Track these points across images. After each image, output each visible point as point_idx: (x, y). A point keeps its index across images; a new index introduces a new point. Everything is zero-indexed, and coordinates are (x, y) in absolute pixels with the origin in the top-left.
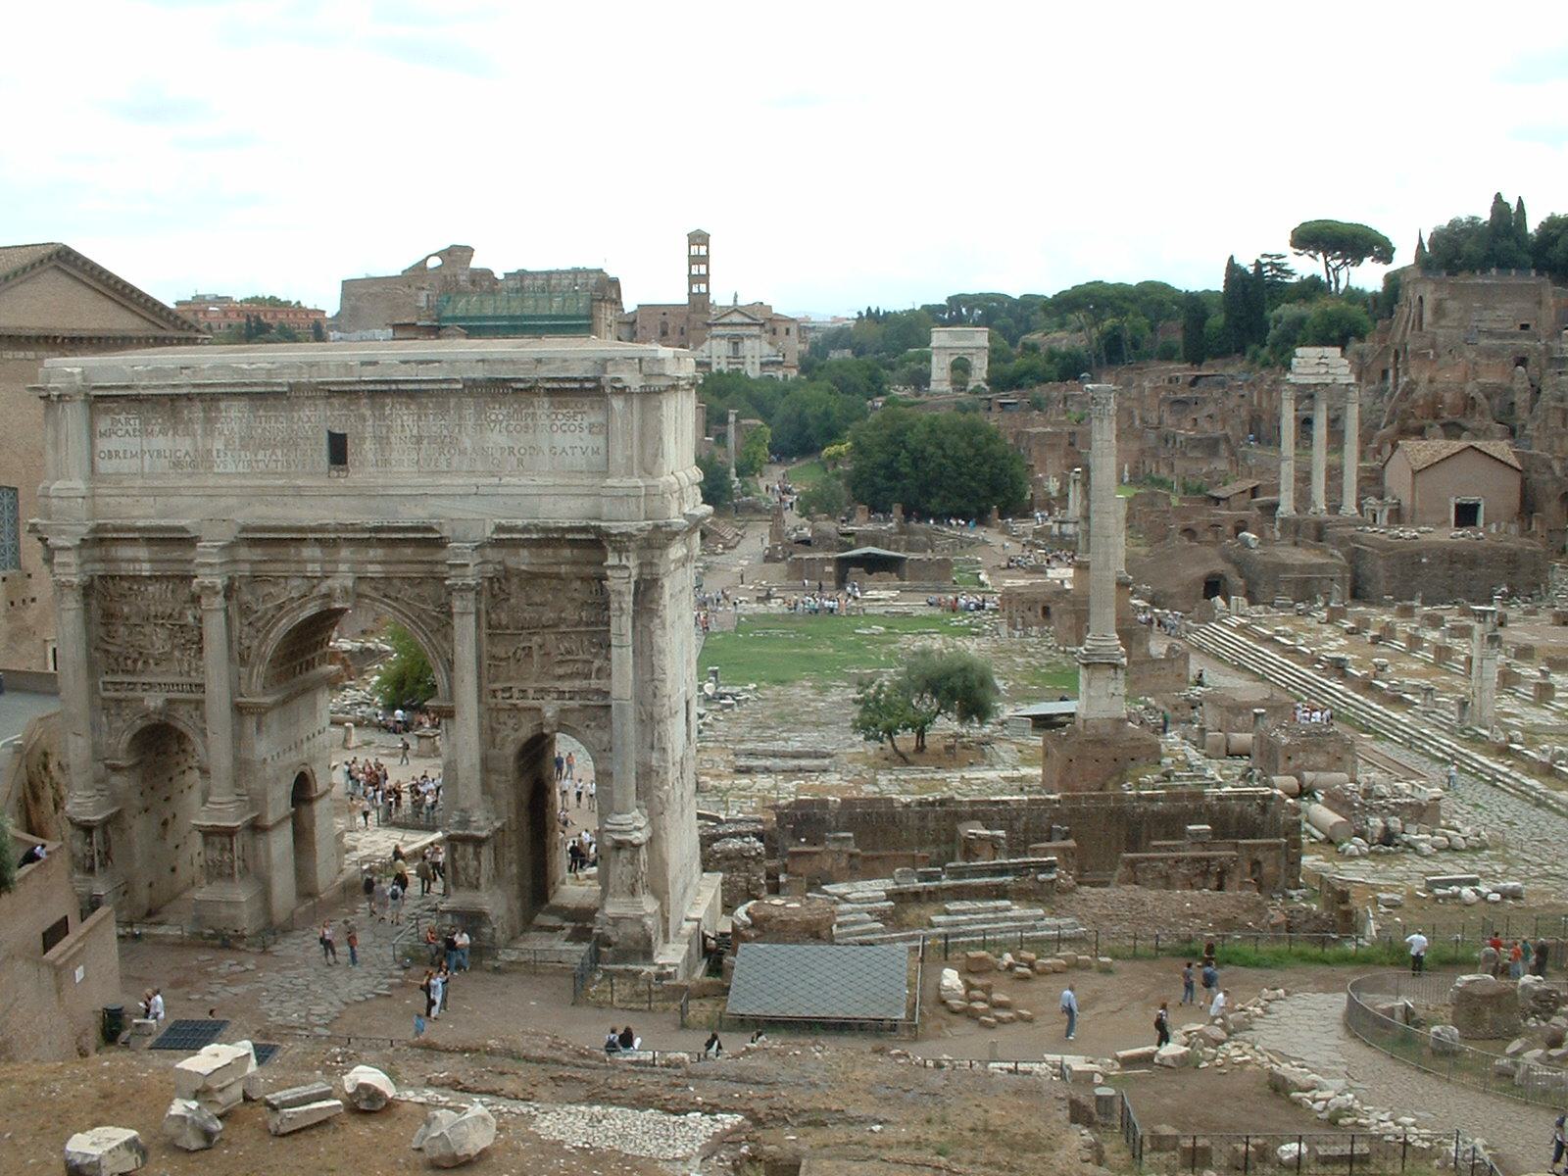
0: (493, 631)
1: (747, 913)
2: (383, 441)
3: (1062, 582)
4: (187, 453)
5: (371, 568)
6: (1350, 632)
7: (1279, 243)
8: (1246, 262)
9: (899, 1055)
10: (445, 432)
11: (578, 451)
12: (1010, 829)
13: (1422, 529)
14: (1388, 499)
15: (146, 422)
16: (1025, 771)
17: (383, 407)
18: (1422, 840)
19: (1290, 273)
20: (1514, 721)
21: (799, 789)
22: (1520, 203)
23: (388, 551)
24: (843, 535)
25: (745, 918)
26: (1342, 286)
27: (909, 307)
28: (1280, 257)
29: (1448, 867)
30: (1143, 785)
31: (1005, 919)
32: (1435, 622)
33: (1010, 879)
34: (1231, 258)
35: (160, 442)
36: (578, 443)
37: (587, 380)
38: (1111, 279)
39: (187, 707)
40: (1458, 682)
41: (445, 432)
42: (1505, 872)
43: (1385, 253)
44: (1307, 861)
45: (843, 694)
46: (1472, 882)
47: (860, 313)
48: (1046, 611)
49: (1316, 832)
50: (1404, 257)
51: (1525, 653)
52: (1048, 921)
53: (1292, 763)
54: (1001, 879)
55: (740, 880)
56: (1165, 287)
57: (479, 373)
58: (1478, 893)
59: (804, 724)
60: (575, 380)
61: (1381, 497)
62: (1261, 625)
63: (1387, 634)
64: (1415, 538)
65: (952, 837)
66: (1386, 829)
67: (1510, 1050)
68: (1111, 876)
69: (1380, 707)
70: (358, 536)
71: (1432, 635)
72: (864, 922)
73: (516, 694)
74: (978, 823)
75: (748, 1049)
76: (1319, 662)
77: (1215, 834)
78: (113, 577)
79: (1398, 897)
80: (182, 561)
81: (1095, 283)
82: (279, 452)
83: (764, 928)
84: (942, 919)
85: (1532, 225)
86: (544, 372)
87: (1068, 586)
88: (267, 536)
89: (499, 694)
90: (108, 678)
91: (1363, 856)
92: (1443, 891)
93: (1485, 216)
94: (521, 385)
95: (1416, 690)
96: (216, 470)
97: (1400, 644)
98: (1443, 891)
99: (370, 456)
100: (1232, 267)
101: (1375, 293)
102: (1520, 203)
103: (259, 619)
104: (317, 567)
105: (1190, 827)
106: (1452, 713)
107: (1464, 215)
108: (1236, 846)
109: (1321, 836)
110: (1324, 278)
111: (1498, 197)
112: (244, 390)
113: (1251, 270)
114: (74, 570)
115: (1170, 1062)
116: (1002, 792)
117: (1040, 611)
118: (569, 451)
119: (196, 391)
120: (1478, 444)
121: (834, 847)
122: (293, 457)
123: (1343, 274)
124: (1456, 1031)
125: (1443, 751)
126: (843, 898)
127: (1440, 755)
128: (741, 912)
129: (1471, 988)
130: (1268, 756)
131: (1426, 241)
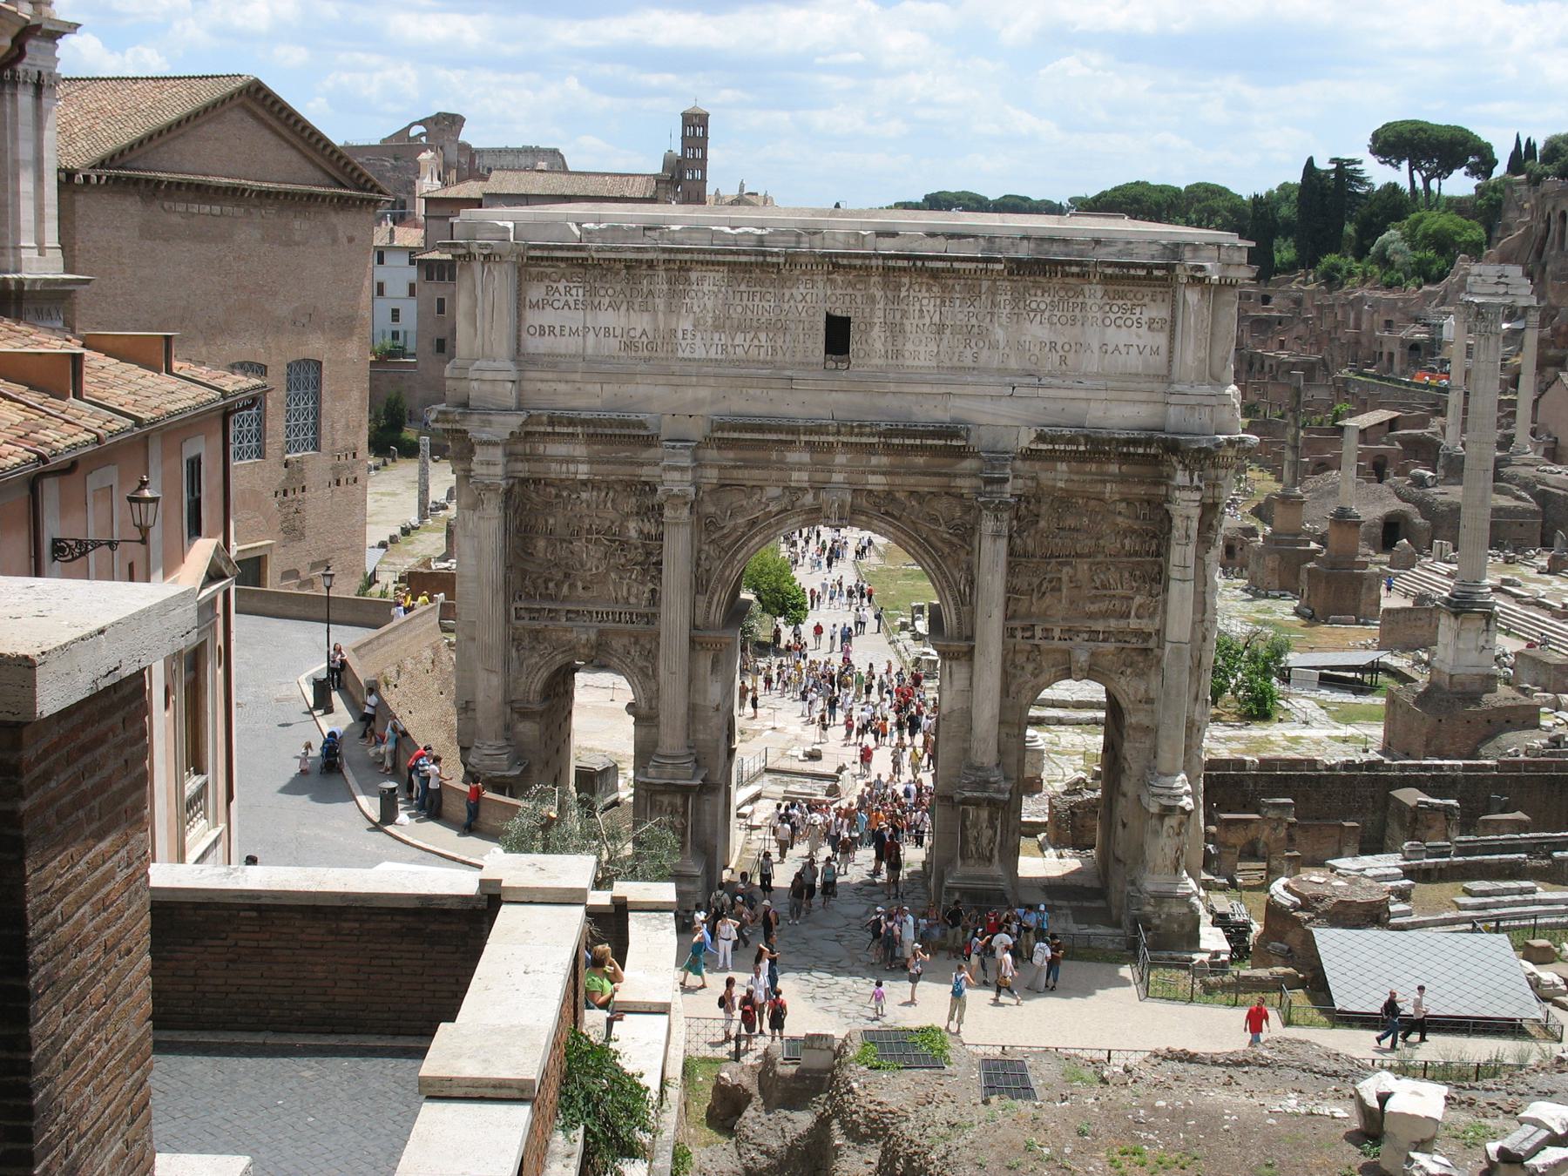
0: (1015, 559)
2: (895, 330)
4: (644, 332)
5: (872, 479)
7: (1358, 150)
10: (974, 321)
11: (1134, 350)
15: (593, 292)
17: (898, 287)
23: (896, 460)
31: (1534, 902)
35: (607, 318)
36: (1135, 341)
37: (1158, 267)
39: (625, 641)
41: (974, 321)
57: (1024, 252)
60: (1143, 266)
70: (864, 440)
73: (1038, 633)
78: (537, 482)
80: (632, 463)
82: (763, 336)
86: (1102, 254)
88: (748, 436)
89: (1019, 634)
90: (520, 605)
94: (1075, 269)
96: (680, 354)
99: (878, 345)
103: (724, 537)
104: (805, 476)
112: (858, 262)
114: (499, 470)
118: (1124, 350)
119: (666, 256)
122: (780, 342)
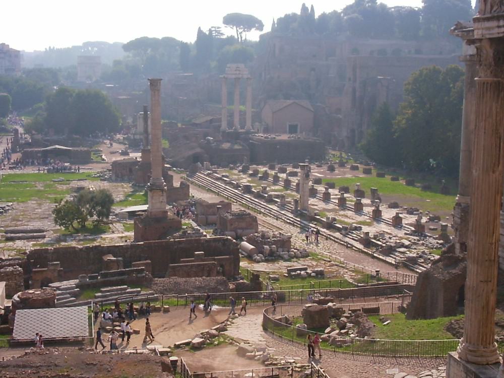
1: (18, 297)
3: (136, 158)
6: (251, 175)
8: (206, 30)
9: (90, 350)
12: (124, 257)
13: (277, 134)
14: (263, 123)
16: (126, 234)
18: (285, 254)
19: (222, 34)
20: (315, 207)
21: (34, 245)
22: (312, 7)
24: (45, 141)
25: (18, 299)
26: (243, 39)
27: (64, 47)
28: (219, 28)
29: (295, 264)
30: (174, 238)
31: (125, 293)
32: (283, 171)
33: (126, 276)
34: (200, 28)
38: (150, 36)
40: (294, 193)
42: (317, 265)
43: (260, 26)
44: (241, 264)
45: (48, 206)
46: (305, 269)
47: (46, 49)
48: (131, 170)
49: (244, 253)
50: (267, 29)
51: (318, 181)
52: (142, 293)
53: (233, 227)
54: (123, 277)
55: (12, 283)
56: (175, 39)
58: (307, 273)
59: (35, 218)
61: (260, 123)
62: (216, 173)
63: (265, 176)
64: (274, 138)
65: (101, 260)
66: (271, 250)
67: (326, 332)
68: (165, 274)
69: (265, 204)
71: (284, 176)
72: (68, 298)
74: (111, 255)
75: (26, 353)
76: (240, 187)
77: (205, 255)
79: (277, 276)
81: (144, 37)
83: (26, 304)
84: (100, 294)
85: (316, 16)
87: (138, 160)
91: (263, 261)
92: (294, 273)
93: (299, 12)
95: (277, 197)
97: (271, 179)
98: (294, 273)
100: (200, 32)
101: (256, 42)
102: (312, 7)
105: (196, 253)
106: (293, 205)
107: (289, 12)
108: (214, 260)
109: (246, 254)
110: (236, 37)
111: (304, 5)
113: (207, 33)
115: (196, 345)
116: (118, 242)
117: (128, 170)
120: (297, 101)
121: (52, 268)
123: (244, 35)
124: (306, 326)
125: (289, 220)
126: (58, 288)
127: (288, 221)
128: (16, 297)
129: (310, 309)
130: (221, 225)
131: (276, 22)
